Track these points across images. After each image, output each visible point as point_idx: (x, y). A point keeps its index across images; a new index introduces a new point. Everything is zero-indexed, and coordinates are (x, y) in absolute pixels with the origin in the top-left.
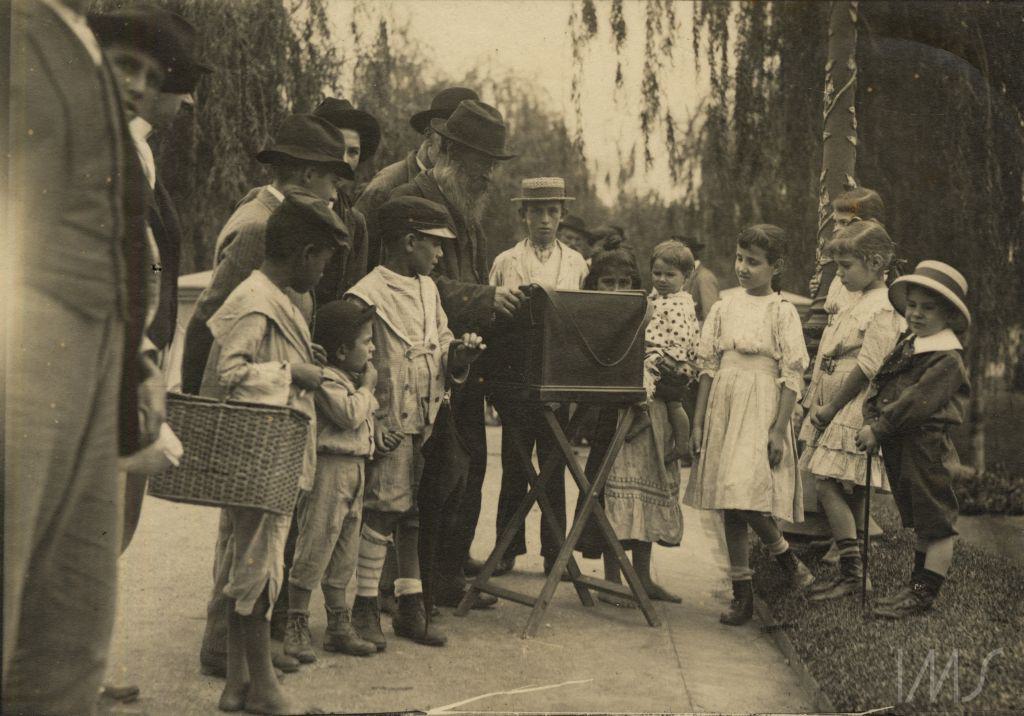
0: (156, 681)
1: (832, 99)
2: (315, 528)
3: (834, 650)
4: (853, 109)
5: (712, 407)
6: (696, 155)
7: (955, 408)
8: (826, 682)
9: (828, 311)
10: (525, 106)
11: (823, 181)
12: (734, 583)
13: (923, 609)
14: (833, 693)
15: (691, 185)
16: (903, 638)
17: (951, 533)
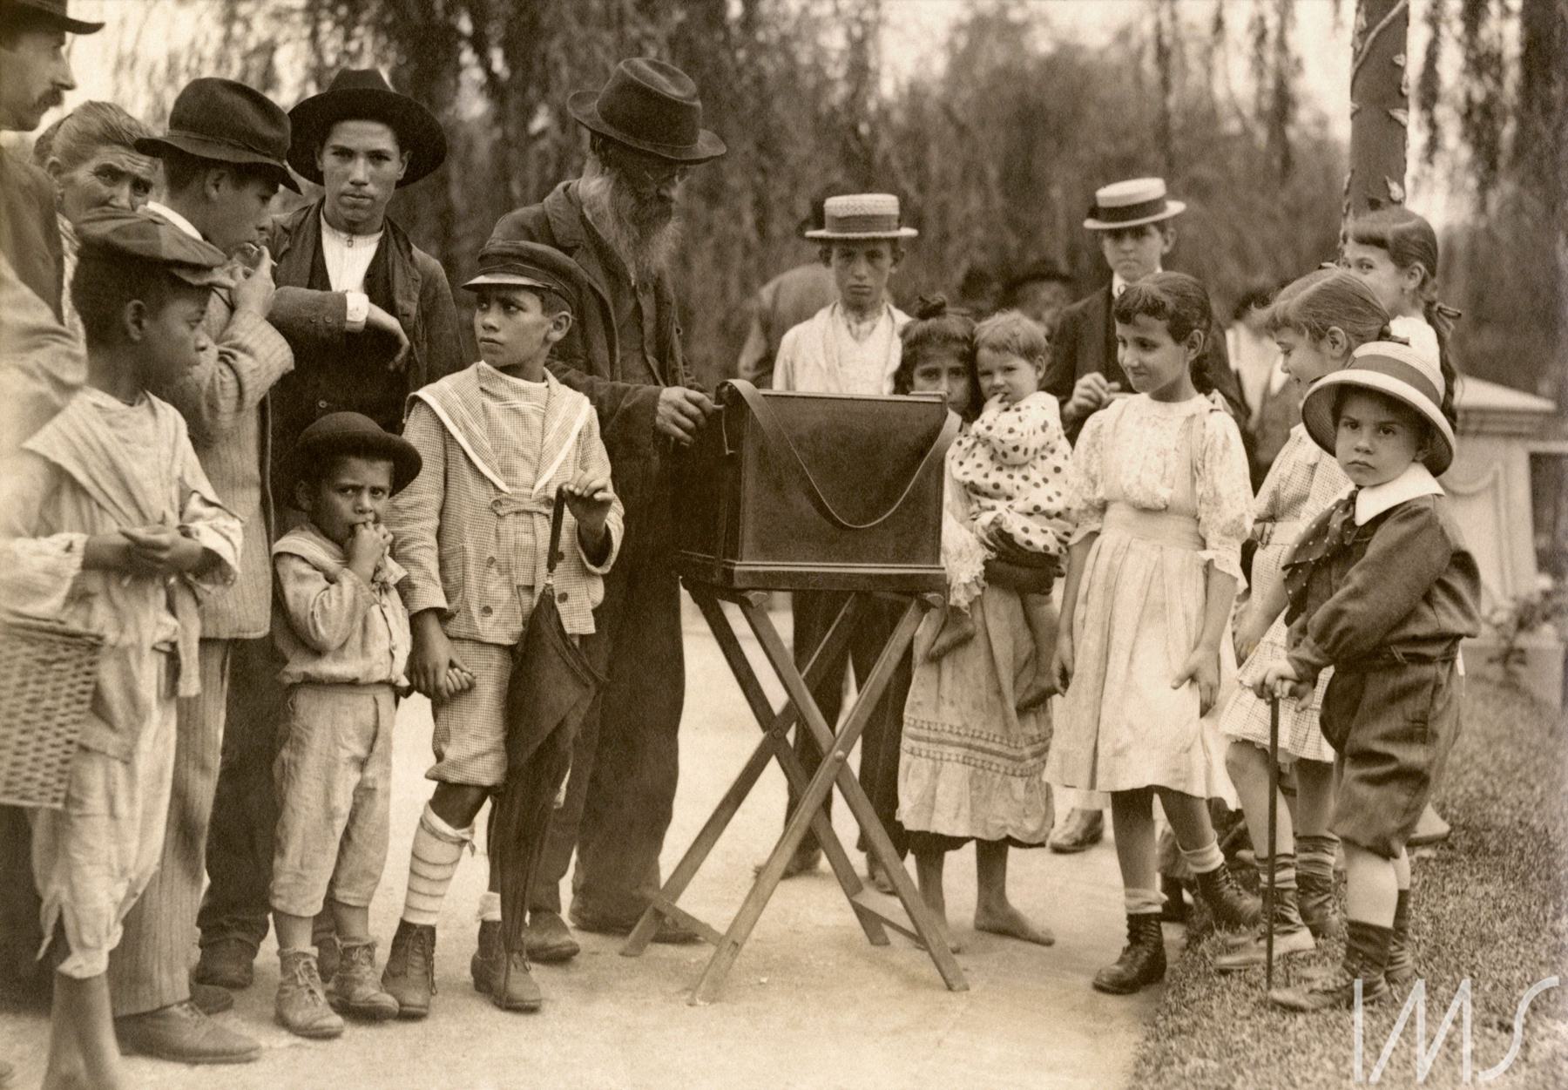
2: (303, 810)
5: (1086, 601)
12: (1131, 917)
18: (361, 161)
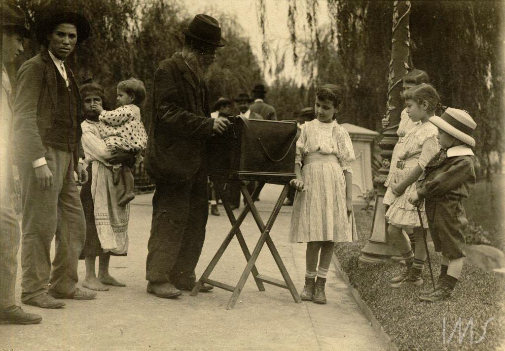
0: (22, 332)
1: (397, 21)
3: (399, 319)
4: (408, 27)
6: (315, 59)
7: (465, 189)
8: (395, 337)
9: (399, 134)
10: (230, 33)
11: (392, 65)
12: (306, 278)
13: (447, 297)
14: (399, 344)
15: (312, 74)
16: (437, 313)
17: (460, 255)
18: (67, 37)
